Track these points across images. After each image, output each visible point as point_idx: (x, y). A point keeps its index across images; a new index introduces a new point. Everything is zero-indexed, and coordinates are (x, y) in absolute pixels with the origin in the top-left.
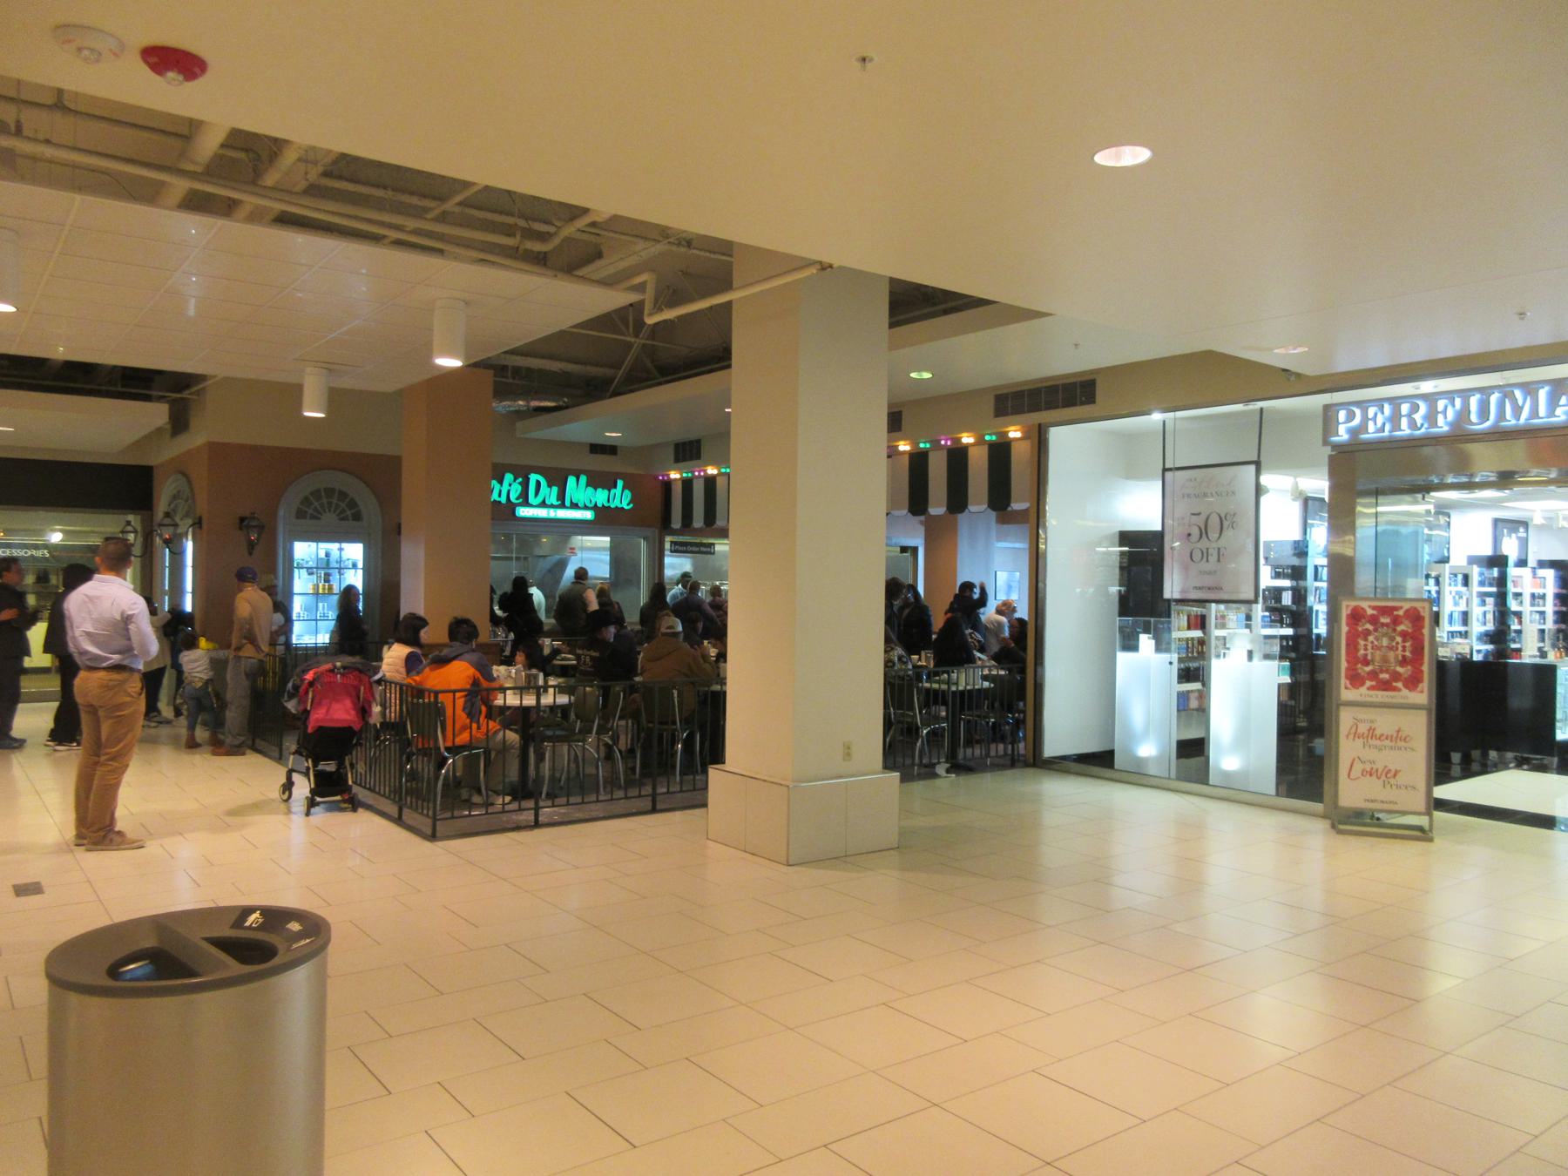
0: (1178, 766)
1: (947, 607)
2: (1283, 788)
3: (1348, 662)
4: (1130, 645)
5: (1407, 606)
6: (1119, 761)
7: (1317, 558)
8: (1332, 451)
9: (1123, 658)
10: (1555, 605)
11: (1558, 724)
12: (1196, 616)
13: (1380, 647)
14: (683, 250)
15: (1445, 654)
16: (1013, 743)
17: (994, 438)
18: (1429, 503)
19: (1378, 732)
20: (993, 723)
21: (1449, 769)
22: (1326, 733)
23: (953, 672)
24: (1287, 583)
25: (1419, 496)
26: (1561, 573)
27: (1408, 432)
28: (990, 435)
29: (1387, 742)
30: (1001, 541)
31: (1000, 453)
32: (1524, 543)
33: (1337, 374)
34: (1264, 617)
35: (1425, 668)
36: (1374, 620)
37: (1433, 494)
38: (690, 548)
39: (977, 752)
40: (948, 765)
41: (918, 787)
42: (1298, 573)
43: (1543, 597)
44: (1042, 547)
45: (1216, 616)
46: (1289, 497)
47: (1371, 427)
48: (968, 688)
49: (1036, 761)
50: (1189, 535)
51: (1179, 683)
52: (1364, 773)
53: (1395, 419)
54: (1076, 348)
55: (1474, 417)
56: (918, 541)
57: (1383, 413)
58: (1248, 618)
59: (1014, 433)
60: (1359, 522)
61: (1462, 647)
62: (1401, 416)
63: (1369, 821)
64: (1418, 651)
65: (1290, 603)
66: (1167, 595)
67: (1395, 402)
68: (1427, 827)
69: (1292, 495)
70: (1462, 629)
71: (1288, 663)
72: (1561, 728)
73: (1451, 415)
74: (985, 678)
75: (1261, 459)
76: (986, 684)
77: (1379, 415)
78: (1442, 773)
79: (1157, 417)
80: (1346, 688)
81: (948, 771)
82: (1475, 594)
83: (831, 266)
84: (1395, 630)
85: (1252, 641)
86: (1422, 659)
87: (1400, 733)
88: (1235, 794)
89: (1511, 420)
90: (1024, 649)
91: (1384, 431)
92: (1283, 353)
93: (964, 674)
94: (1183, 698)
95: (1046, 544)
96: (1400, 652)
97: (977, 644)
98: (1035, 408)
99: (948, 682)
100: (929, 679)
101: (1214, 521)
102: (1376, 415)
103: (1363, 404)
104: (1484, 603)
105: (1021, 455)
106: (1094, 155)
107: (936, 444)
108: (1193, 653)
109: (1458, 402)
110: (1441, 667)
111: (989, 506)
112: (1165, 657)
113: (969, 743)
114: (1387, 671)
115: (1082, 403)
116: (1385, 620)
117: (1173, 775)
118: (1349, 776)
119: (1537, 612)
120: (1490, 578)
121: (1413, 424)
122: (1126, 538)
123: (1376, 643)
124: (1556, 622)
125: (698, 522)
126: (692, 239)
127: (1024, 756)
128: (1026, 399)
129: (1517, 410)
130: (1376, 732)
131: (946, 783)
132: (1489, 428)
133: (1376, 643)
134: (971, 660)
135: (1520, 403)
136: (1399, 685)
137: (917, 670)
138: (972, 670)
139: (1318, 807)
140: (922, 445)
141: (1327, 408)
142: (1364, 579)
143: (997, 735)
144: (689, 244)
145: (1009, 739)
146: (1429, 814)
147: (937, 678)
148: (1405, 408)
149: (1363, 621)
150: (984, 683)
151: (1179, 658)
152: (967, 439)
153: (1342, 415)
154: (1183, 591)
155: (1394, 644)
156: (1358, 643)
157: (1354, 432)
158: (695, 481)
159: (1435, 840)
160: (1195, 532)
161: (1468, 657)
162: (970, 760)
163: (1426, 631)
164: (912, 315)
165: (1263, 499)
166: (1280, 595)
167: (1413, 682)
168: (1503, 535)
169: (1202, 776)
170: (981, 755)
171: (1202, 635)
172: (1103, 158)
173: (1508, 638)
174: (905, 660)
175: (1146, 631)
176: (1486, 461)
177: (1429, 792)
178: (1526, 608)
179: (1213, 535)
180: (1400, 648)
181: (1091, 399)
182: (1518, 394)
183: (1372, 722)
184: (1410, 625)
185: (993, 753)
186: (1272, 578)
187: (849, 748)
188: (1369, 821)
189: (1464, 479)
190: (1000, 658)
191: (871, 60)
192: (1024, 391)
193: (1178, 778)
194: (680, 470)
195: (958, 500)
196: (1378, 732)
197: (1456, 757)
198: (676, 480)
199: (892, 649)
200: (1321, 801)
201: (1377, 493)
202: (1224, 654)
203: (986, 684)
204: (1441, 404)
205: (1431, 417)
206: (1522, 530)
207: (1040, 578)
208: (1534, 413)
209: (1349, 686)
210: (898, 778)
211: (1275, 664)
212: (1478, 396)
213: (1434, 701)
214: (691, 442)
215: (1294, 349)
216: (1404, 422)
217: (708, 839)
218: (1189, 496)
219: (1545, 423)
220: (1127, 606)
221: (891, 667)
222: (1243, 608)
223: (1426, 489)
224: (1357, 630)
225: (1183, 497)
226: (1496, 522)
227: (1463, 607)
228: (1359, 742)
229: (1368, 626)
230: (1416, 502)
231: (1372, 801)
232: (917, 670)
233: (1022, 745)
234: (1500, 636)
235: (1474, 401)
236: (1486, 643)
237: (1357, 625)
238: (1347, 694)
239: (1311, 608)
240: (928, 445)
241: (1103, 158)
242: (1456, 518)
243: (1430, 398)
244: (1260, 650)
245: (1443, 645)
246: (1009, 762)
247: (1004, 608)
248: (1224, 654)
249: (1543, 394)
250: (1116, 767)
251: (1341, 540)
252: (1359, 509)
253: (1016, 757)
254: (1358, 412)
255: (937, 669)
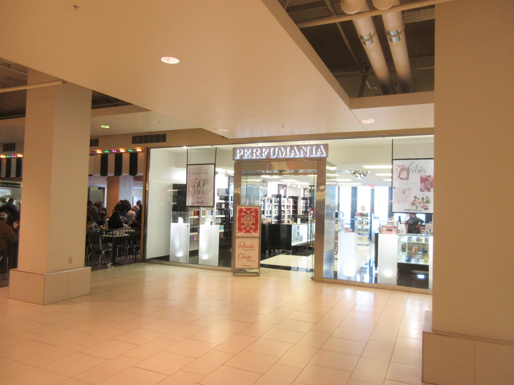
0: (189, 259)
1: (114, 209)
2: (221, 264)
3: (238, 225)
4: (175, 220)
5: (254, 208)
6: (171, 259)
7: (231, 194)
8: (235, 161)
9: (173, 225)
10: (293, 209)
11: (292, 241)
12: (197, 211)
13: (248, 221)
14: (6, 68)
15: (265, 222)
16: (136, 255)
17: (132, 151)
18: (260, 179)
19: (246, 245)
20: (129, 248)
21: (265, 255)
22: (232, 247)
23: (115, 231)
24: (223, 201)
25: (258, 176)
26: (294, 200)
27: (255, 157)
28: (131, 149)
29: (248, 248)
30: (135, 187)
31: (134, 156)
32: (285, 191)
33: (238, 139)
34: (216, 212)
35: (259, 226)
36: (246, 212)
37: (261, 176)
38: (9, 185)
39: (123, 258)
40: (112, 264)
41: (101, 272)
42: (226, 198)
43: (290, 206)
44: (147, 189)
45: (202, 211)
46: (224, 175)
47: (246, 155)
48: (120, 236)
49: (144, 260)
50: (194, 186)
51: (190, 233)
52: (242, 258)
53: (252, 153)
54: (159, 123)
55: (272, 155)
56: (105, 186)
57: (249, 151)
58: (212, 212)
59: (139, 150)
60: (242, 184)
61: (269, 220)
62: (253, 153)
63: (243, 272)
64: (257, 221)
65: (224, 208)
66: (187, 205)
67: (251, 148)
68: (258, 272)
69: (225, 175)
70: (270, 215)
71: (223, 226)
72: (293, 242)
73: (266, 153)
74: (126, 233)
75: (216, 163)
76: (126, 235)
77: (248, 152)
78: (263, 256)
79: (185, 148)
80: (238, 232)
81: (112, 266)
82: (273, 206)
83: (67, 82)
84: (251, 215)
85: (212, 219)
86: (258, 223)
87: (252, 245)
88: (207, 267)
89: (280, 156)
90: (140, 222)
91: (249, 157)
92: (221, 131)
93: (119, 231)
94: (191, 237)
95: (148, 188)
96: (252, 221)
97: (125, 221)
98: (146, 142)
99: (113, 234)
100: (106, 234)
101: (202, 182)
102: (247, 152)
103: (244, 148)
104: (275, 208)
105: (141, 157)
106: (161, 58)
107: (111, 151)
108: (195, 223)
109: (268, 150)
110: (263, 226)
111: (129, 174)
112: (186, 224)
113: (120, 255)
114: (249, 227)
115: (162, 142)
116: (248, 212)
117: (188, 262)
118: (238, 259)
119: (288, 210)
120: (277, 201)
121: (256, 155)
122: (175, 186)
123: (246, 219)
124: (293, 213)
125: (13, 175)
126: (10, 64)
127: (140, 259)
128: (143, 139)
129: (282, 153)
130: (246, 245)
131: (111, 270)
132: (275, 158)
133: (246, 219)
134: (122, 226)
135: (283, 151)
136: (252, 231)
137: (101, 230)
138: (121, 230)
139: (229, 269)
140: (106, 152)
141: (234, 149)
142: (243, 201)
143: (131, 252)
144: (9, 66)
145: (134, 254)
146: (259, 268)
147: (109, 233)
148: (255, 150)
149: (243, 212)
150: (126, 234)
151: (191, 225)
152: (122, 150)
153: (238, 151)
154: (192, 203)
155: (251, 219)
156: (241, 219)
157: (241, 156)
158: (12, 160)
159: (261, 276)
160: (196, 185)
161: (271, 223)
162: (120, 261)
163: (259, 215)
164: (103, 105)
165: (216, 176)
166: (221, 205)
167: (255, 230)
168: (280, 189)
169: (197, 262)
170: (124, 259)
171: (198, 217)
172: (164, 60)
173: (281, 218)
174: (97, 227)
175: (181, 216)
176: (277, 167)
177: (259, 262)
178: (286, 209)
179: (201, 185)
180: (252, 220)
181: (164, 140)
182: (282, 149)
183: (244, 242)
184: (255, 213)
185: (128, 258)
186: (219, 200)
187: (71, 259)
188: (243, 272)
189: (271, 172)
190: (132, 226)
191: (79, 7)
192: (154, 135)
193: (190, 263)
194: (6, 155)
195: (118, 171)
196: (246, 245)
197: (267, 252)
198: (4, 158)
199: (92, 223)
200: (231, 267)
201: (247, 175)
202: (204, 223)
203: (126, 235)
204: (264, 150)
205: (261, 154)
206: (285, 188)
207: (146, 199)
208: (286, 154)
209: (239, 232)
210: (91, 269)
211: (219, 226)
212: (273, 148)
213: (261, 236)
214: (11, 144)
215: (225, 130)
216: (254, 154)
217: (9, 298)
218: (195, 173)
219: (289, 157)
220: (175, 208)
221: (91, 229)
222: (211, 209)
223: (260, 174)
224: (241, 215)
225: (193, 174)
226: (279, 185)
227: (270, 209)
228: (241, 248)
229: (244, 214)
230: (257, 179)
231: (244, 266)
232: (101, 230)
233: (139, 255)
234: (279, 217)
235: (272, 149)
236: (276, 219)
237: (241, 214)
238: (238, 234)
239: (230, 209)
240: (108, 152)
241: (164, 60)
242: (269, 184)
243: (261, 148)
244: (214, 222)
245: (265, 220)
246: (134, 261)
247: (134, 208)
248: (204, 223)
249: (288, 149)
250: (170, 261)
251: (237, 189)
252: (242, 180)
253: (136, 259)
254: (242, 150)
255: (109, 230)
